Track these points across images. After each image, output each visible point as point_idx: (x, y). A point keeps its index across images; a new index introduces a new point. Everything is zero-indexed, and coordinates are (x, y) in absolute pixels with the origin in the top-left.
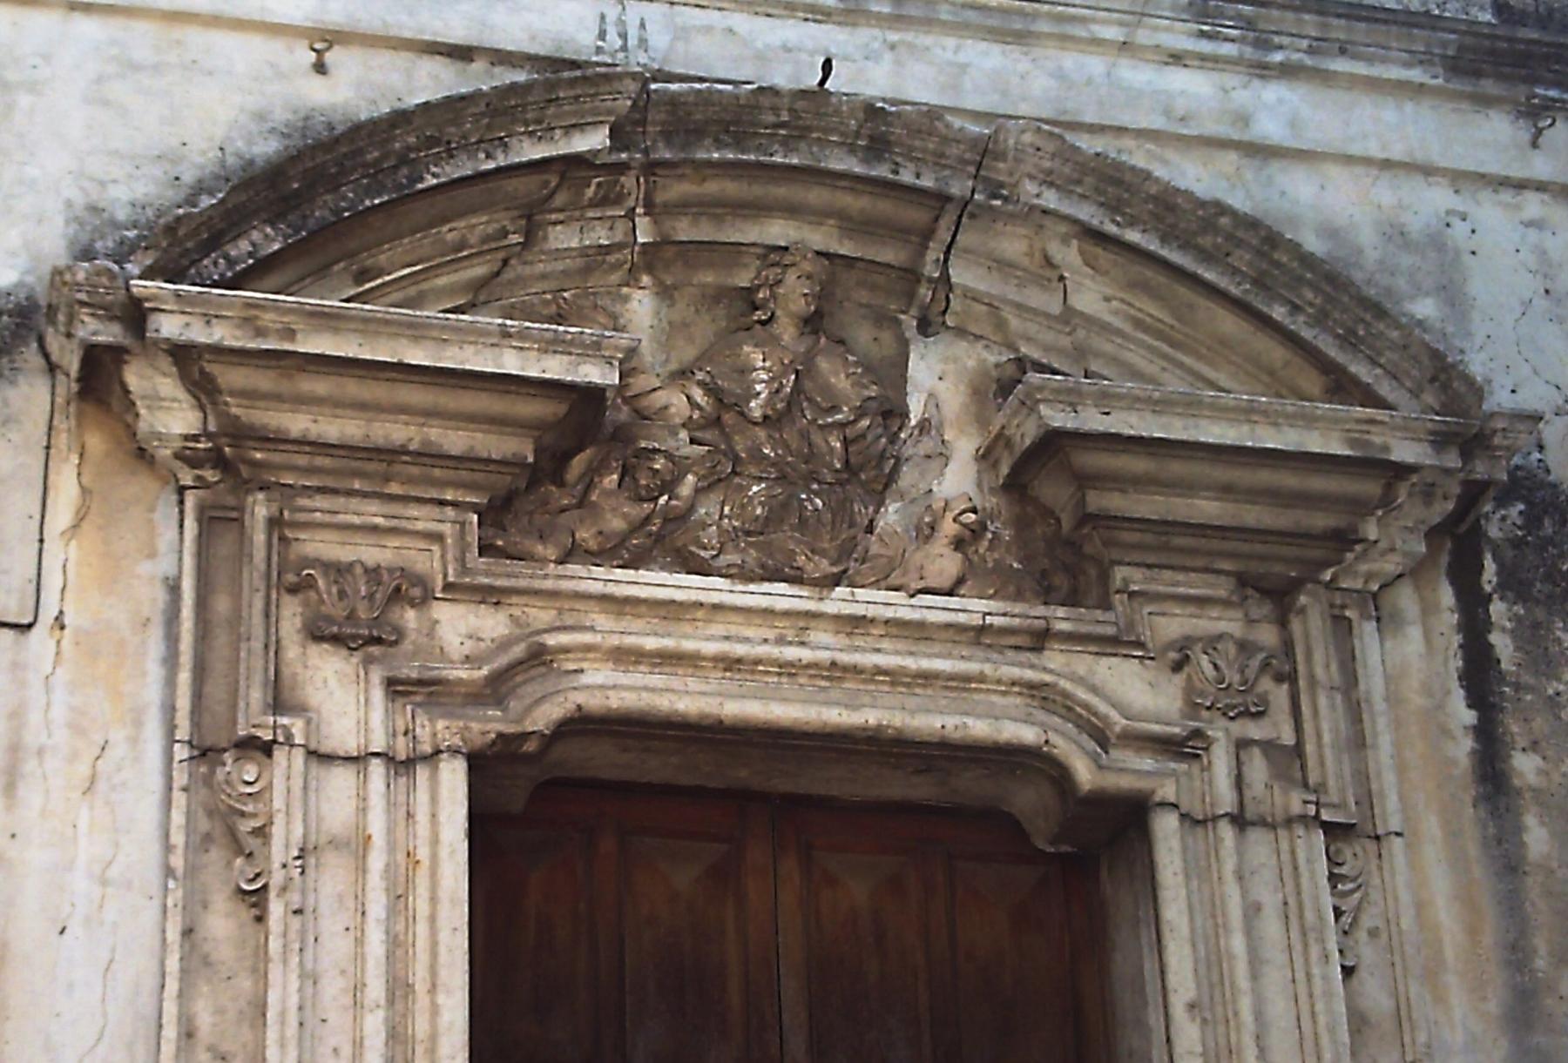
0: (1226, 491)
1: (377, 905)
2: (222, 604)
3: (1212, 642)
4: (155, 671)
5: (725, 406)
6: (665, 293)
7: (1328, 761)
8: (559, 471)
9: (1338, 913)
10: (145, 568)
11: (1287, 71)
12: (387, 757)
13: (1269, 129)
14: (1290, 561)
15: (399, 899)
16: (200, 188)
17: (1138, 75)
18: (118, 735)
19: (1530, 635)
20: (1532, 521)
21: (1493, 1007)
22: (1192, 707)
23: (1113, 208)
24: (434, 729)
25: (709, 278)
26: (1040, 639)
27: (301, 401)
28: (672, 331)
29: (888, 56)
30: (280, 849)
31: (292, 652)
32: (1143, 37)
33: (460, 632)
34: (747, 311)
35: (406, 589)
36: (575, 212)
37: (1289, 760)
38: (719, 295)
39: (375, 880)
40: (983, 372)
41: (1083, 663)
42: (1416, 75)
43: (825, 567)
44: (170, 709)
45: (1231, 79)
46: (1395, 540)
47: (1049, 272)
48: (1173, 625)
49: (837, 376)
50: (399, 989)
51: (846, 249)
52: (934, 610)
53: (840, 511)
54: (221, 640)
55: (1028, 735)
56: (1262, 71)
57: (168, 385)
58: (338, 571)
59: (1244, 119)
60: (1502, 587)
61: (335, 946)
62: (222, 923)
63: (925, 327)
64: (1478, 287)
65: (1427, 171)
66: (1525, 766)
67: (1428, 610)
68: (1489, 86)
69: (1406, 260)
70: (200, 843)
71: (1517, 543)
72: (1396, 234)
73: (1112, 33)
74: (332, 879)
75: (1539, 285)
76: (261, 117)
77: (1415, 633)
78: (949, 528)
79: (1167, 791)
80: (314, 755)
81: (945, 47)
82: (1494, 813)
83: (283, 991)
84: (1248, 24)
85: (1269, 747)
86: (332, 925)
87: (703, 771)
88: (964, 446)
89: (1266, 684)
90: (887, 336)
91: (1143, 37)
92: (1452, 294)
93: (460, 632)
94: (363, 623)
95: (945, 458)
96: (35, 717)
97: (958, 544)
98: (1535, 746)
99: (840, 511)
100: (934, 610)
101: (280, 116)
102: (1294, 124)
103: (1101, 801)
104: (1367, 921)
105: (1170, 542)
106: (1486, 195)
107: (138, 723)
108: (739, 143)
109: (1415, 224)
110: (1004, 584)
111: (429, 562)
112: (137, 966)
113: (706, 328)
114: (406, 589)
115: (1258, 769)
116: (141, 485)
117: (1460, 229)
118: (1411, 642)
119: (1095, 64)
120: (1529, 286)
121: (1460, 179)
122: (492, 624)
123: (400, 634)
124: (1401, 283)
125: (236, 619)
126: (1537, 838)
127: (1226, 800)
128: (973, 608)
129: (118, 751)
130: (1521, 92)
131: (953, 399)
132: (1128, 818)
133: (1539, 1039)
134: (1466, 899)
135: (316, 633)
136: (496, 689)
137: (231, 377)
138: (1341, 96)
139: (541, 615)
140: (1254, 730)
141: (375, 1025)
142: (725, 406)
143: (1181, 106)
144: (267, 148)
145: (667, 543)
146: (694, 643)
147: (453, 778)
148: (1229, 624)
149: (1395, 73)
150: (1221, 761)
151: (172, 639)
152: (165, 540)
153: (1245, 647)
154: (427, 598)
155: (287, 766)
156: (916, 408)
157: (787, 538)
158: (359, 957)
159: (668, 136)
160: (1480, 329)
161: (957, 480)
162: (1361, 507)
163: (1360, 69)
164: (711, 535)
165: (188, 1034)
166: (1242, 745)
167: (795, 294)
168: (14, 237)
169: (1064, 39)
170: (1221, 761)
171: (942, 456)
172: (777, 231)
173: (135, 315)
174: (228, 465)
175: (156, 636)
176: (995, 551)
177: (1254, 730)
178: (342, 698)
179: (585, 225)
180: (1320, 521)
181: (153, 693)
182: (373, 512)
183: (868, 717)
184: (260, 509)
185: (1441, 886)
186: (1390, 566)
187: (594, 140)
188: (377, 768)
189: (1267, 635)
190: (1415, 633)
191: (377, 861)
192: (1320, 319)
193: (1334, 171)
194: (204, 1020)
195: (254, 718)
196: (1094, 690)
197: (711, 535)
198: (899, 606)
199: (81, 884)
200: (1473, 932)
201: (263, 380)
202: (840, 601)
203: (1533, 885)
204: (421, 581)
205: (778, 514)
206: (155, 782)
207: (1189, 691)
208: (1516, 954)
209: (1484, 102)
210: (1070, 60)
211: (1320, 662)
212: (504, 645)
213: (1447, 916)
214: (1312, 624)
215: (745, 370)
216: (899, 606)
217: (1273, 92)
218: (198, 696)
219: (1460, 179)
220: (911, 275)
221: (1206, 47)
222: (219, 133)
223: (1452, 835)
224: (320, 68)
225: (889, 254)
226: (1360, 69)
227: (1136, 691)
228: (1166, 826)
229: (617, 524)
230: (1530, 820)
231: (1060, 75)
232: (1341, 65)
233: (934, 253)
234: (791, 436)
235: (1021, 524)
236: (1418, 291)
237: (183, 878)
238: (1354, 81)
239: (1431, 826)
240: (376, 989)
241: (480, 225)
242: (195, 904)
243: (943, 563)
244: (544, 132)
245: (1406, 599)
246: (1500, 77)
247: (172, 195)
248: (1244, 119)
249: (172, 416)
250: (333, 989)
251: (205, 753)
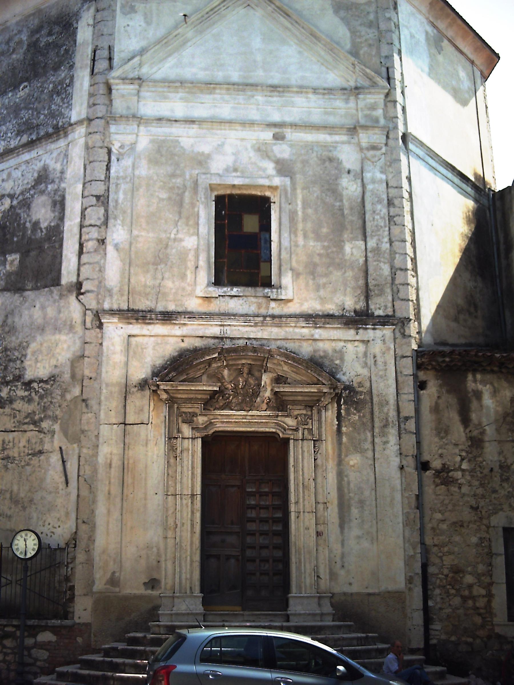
0: (302, 396)
1: (190, 458)
2: (172, 418)
3: (300, 415)
4: (163, 428)
5: (236, 386)
6: (229, 370)
7: (315, 431)
8: (211, 401)
9: (315, 451)
10: (162, 415)
11: (320, 327)
12: (192, 438)
13: (317, 337)
14: (313, 404)
15: (193, 456)
16: (167, 361)
17: (297, 330)
18: (159, 437)
19: (347, 410)
20: (350, 393)
21: (335, 463)
22: (298, 424)
23: (287, 358)
24: (198, 435)
25: (235, 367)
26: (277, 416)
27: (180, 393)
28: (230, 375)
29: (261, 332)
30: (178, 451)
31: (180, 424)
32: (298, 325)
33: (201, 420)
34: (240, 373)
35: (195, 415)
36: (215, 362)
37: (310, 431)
38: (236, 369)
39: (190, 454)
40: (272, 378)
41: (283, 419)
42: (339, 326)
43: (248, 409)
44: (165, 433)
45: (311, 329)
46: (325, 401)
47: (280, 365)
48: (296, 412)
49: (252, 381)
50: (193, 468)
51: (253, 363)
52: (263, 413)
53: (251, 400)
54: (171, 423)
55: (274, 430)
56: (316, 328)
57: (163, 393)
58: (185, 413)
59: (313, 335)
60: (344, 403)
61: (186, 463)
62: (172, 460)
63: (265, 372)
64: (346, 358)
65: (340, 340)
66: (344, 429)
67: (333, 408)
68: (350, 326)
69: (336, 355)
70: (169, 450)
71: (347, 397)
72: (335, 351)
73: (293, 325)
74: (185, 454)
75: (355, 356)
76: (175, 349)
77: (330, 411)
78: (265, 401)
79: (292, 437)
80: (182, 438)
81: (269, 329)
82: (339, 436)
83: (179, 469)
84: (314, 321)
85: (308, 429)
86: (185, 460)
87: (234, 434)
88: (269, 389)
89: (308, 420)
90: (260, 373)
91: (298, 325)
92: (342, 359)
93: (201, 420)
94: (189, 419)
95: (266, 391)
96: (149, 436)
97: (267, 403)
98: (346, 426)
99: (251, 400)
100: (263, 413)
101: (178, 349)
102: (320, 335)
103: (283, 439)
104: (319, 452)
105: (295, 403)
106: (349, 343)
107: (161, 435)
108: (236, 353)
109: (337, 349)
110: (273, 409)
111: (198, 411)
112: (162, 467)
113: (235, 374)
114: (195, 415)
115: (306, 432)
116: (160, 404)
117: (345, 348)
118: (329, 413)
119: (291, 329)
120: (354, 357)
121: (345, 341)
122: (205, 419)
123: (193, 421)
124: (334, 358)
125: (173, 421)
126: (344, 439)
127: (300, 437)
128: (268, 413)
129: (159, 439)
130: (355, 326)
131: (268, 382)
132: (286, 441)
133: (342, 467)
134: (333, 449)
135: (184, 422)
136: (206, 428)
137: (170, 392)
138: (329, 330)
139: (212, 417)
140: (306, 427)
141: (190, 472)
142: (236, 388)
143: (303, 335)
144: (176, 354)
145: (227, 406)
146: (232, 420)
147: (200, 441)
148: (304, 412)
149: (336, 326)
150: (300, 432)
151: (165, 424)
152: (164, 410)
153: (305, 415)
154: (197, 416)
155: (179, 440)
156: (263, 383)
157: (244, 405)
158: (188, 464)
159: (226, 353)
160: (345, 364)
161: (268, 394)
162: (321, 396)
163: (331, 326)
164: (234, 405)
165: (168, 475)
166: (304, 429)
167: (246, 370)
168: (144, 371)
169: (286, 326)
170: (300, 432)
171: (266, 390)
172: (244, 361)
173: (158, 386)
174: (172, 401)
175: (164, 423)
176: (273, 404)
177: (306, 427)
178: (186, 430)
179: (217, 363)
180: (315, 398)
181: (163, 431)
182: (190, 405)
183: (253, 429)
184: (176, 406)
185: (330, 447)
186: (326, 403)
187: (216, 355)
188: (190, 440)
189: (309, 413)
190: (330, 411)
191: (190, 452)
192: (315, 372)
193: (326, 342)
194: (170, 473)
195: (175, 435)
196: (284, 423)
197: (234, 405)
198: (259, 413)
199: (155, 457)
200: (334, 453)
201: (174, 392)
202: (250, 413)
203: (343, 446)
204: (196, 414)
205: (243, 400)
206: (163, 440)
207: (298, 422)
208: (339, 456)
209: (350, 328)
210: (287, 329)
211: (315, 417)
212: (207, 422)
213: (330, 451)
214: (315, 411)
215: (239, 381)
216: (259, 413)
217: (317, 331)
218: (169, 431)
219: (345, 341)
220: (262, 366)
221: (307, 325)
222: (170, 352)
223: (332, 439)
224: (183, 341)
225: (259, 363)
226: (331, 326)
227: (291, 422)
228: (291, 442)
229: (222, 404)
230: (344, 437)
231: (286, 332)
232: (328, 326)
233: (265, 362)
234: (245, 390)
235: (276, 399)
236: (337, 359)
237: (167, 456)
238: (330, 328)
239: (330, 439)
240: (190, 468)
241: (203, 366)
242: (169, 458)
243: (264, 406)
244: (209, 355)
245: (330, 406)
246: (352, 324)
247: (164, 362)
248: (313, 335)
249: (164, 396)
250: (185, 468)
251: (170, 438)
